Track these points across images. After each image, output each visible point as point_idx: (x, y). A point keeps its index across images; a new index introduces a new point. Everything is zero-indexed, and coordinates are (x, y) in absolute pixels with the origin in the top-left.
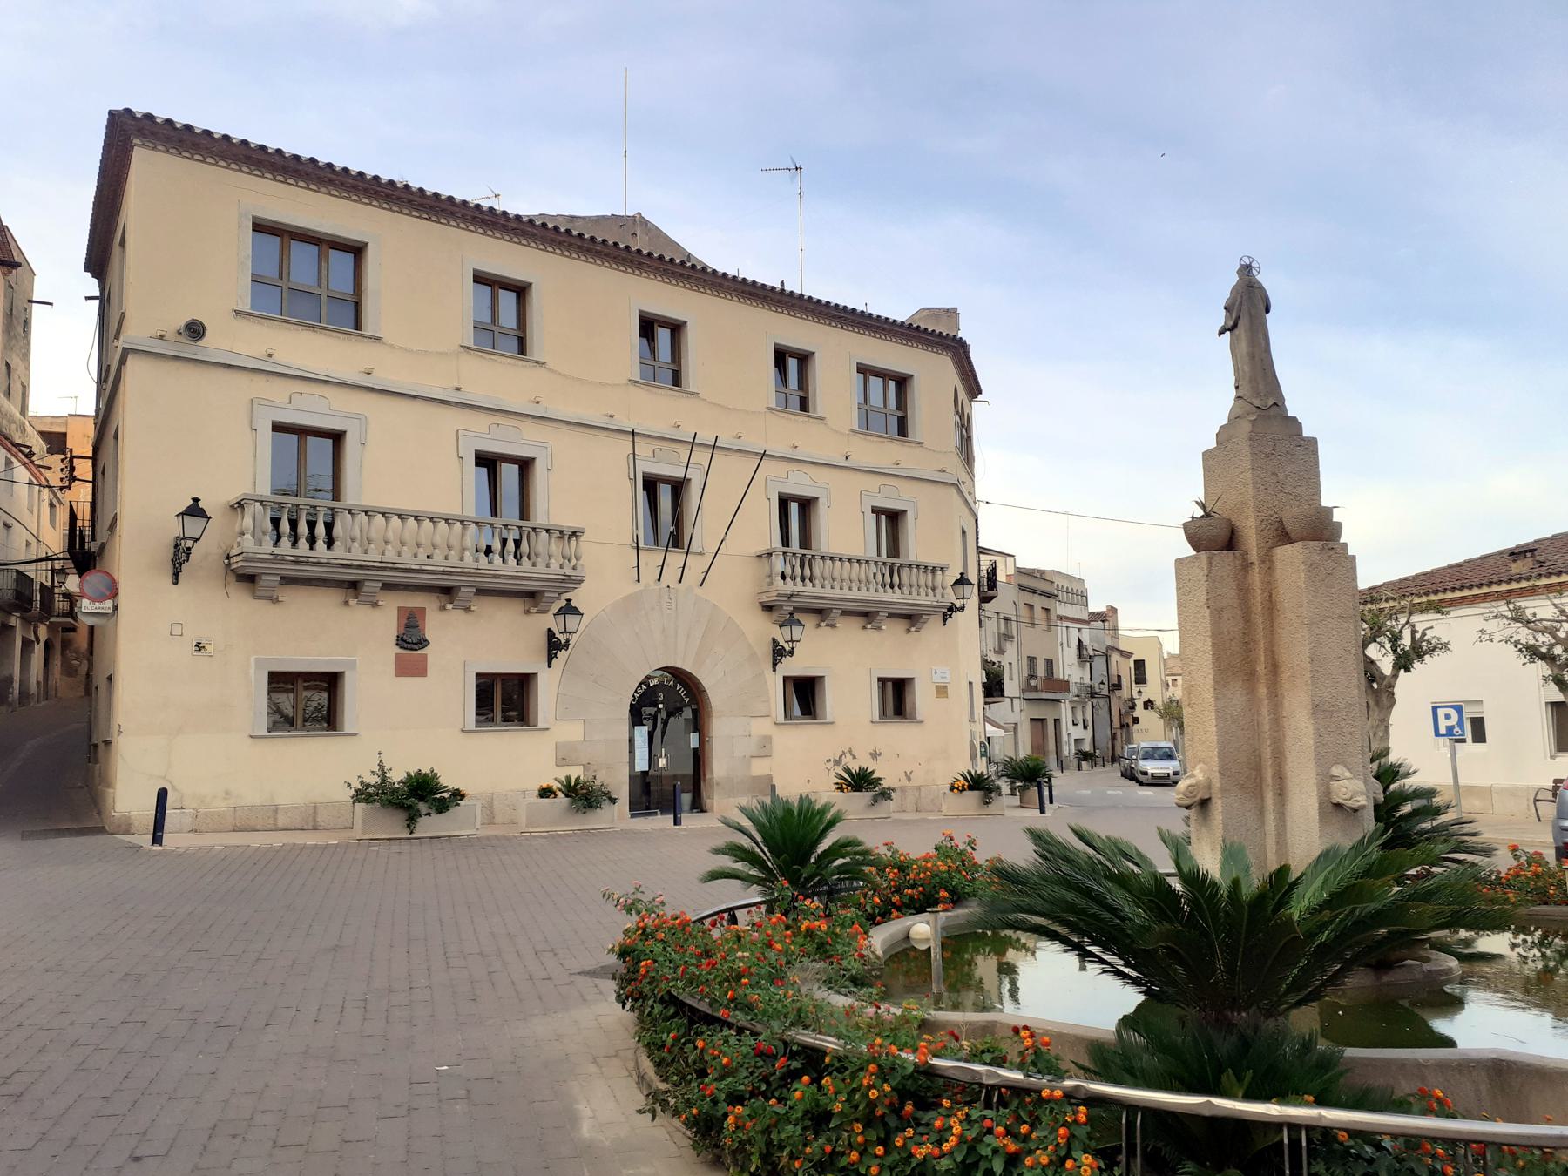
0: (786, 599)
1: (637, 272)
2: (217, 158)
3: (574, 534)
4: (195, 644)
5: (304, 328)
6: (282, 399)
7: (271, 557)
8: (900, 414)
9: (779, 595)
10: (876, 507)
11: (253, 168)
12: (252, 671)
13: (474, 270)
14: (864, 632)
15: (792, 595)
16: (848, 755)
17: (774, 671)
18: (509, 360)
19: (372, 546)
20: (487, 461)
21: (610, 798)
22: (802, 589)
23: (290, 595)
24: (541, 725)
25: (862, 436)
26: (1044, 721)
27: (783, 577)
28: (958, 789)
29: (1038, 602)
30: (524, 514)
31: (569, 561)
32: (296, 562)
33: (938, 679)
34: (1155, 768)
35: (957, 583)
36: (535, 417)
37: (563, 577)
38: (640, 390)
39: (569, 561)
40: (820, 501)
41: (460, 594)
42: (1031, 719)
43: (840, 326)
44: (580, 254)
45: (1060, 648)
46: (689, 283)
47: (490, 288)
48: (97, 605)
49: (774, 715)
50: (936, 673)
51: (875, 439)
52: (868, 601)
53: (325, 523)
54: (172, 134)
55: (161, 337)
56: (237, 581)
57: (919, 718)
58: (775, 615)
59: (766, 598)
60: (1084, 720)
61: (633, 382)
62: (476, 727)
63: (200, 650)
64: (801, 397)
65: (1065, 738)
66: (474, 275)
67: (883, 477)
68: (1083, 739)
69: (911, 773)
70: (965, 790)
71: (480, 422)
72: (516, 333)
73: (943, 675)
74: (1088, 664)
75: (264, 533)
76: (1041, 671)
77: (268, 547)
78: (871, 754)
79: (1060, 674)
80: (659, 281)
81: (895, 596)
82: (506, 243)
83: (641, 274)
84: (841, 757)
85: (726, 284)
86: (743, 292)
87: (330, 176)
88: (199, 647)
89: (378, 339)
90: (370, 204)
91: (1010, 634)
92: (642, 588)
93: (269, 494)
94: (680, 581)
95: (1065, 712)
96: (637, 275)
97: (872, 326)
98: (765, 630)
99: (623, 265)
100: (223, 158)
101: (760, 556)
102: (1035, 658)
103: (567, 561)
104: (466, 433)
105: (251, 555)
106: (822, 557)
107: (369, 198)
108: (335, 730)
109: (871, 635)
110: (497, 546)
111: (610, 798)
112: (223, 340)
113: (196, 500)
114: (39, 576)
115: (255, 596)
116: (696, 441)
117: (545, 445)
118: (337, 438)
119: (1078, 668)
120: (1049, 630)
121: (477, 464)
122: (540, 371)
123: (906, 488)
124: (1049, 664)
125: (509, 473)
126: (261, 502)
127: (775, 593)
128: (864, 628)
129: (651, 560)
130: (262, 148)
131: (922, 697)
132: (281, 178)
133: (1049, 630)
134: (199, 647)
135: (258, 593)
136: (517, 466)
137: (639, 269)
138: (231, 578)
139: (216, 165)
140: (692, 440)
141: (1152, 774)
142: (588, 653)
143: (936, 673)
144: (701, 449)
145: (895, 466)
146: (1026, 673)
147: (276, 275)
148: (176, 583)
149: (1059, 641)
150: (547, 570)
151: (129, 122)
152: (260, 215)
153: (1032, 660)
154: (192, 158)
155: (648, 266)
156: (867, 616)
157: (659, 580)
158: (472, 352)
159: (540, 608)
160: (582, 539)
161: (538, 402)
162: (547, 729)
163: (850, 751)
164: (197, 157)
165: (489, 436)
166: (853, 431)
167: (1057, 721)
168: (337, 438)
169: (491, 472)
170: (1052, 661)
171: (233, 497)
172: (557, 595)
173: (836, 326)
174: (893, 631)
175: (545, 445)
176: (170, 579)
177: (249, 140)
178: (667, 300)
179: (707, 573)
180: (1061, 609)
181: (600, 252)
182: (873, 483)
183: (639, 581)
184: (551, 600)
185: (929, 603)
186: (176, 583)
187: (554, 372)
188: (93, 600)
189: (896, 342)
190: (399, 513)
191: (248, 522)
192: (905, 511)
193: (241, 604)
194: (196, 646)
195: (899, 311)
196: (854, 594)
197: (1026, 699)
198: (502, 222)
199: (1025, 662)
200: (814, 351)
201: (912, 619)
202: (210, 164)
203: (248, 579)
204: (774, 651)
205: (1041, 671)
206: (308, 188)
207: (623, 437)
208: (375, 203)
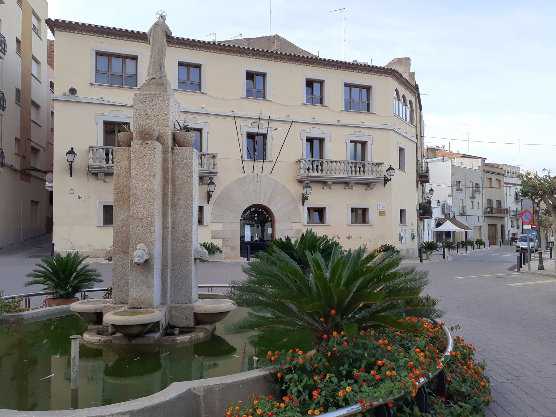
0: (306, 178)
1: (245, 56)
2: (83, 32)
3: (380, 164)
4: (78, 196)
5: (114, 88)
6: (107, 113)
7: (209, 172)
8: (367, 102)
9: (302, 177)
10: (308, 137)
11: (95, 33)
12: (98, 205)
13: (179, 62)
14: (324, 190)
15: (308, 177)
16: (336, 237)
17: (303, 205)
18: (192, 93)
19: (374, 173)
20: (310, 140)
21: (220, 251)
22: (313, 174)
23: (334, 187)
24: (205, 224)
25: (346, 112)
26: (496, 225)
27: (308, 169)
28: (377, 251)
29: (494, 177)
30: (321, 156)
31: (379, 173)
32: (108, 168)
33: (381, 208)
34: (522, 245)
35: (388, 169)
36: (202, 113)
37: (209, 172)
38: (247, 101)
39: (379, 173)
40: (326, 139)
41: (328, 184)
42: (488, 225)
43: (337, 69)
44: (221, 51)
45: (505, 196)
46: (267, 58)
47: (187, 67)
48: (50, 184)
49: (303, 222)
50: (380, 206)
51: (353, 113)
52: (344, 178)
53: (316, 165)
54: (65, 25)
55: (64, 95)
56: (92, 175)
57: (370, 223)
58: (304, 184)
59: (299, 178)
60: (517, 225)
61: (243, 98)
62: (103, 225)
63: (79, 198)
64: (368, 103)
65: (507, 232)
66: (306, 80)
67: (356, 128)
68: (517, 233)
69: (366, 245)
70: (381, 252)
71: (307, 128)
72: (320, 97)
73: (383, 207)
74: (521, 202)
75: (103, 159)
76: (495, 206)
77: (104, 163)
78: (347, 237)
79: (505, 206)
80: (255, 58)
81: (356, 175)
82: (279, 63)
83: (340, 69)
84: (333, 238)
85: (283, 57)
86: (291, 59)
87: (122, 33)
88: (79, 197)
89: (270, 101)
90: (138, 42)
91: (479, 190)
92: (246, 175)
93: (103, 145)
94: (262, 172)
95: (507, 222)
96: (245, 57)
97: (378, 71)
98: (299, 190)
99: (239, 54)
100: (84, 31)
101: (297, 162)
102: (492, 200)
103: (378, 173)
104: (100, 114)
105: (91, 166)
106: (368, 163)
107: (137, 39)
108: (323, 224)
109: (348, 191)
110: (311, 167)
111: (220, 251)
112: (81, 94)
113: (72, 148)
114: (478, 189)
115: (98, 180)
116: (270, 119)
117: (206, 123)
118: (200, 130)
119: (515, 204)
120: (500, 189)
121: (307, 141)
122: (205, 96)
123: (367, 132)
124: (499, 203)
125: (316, 143)
126: (209, 155)
127: (300, 176)
128: (345, 188)
129: (249, 165)
130: (96, 26)
131: (372, 216)
132: (106, 36)
133: (500, 189)
134: (79, 197)
135: (99, 179)
136: (319, 141)
137: (245, 55)
138: (90, 174)
139: (82, 34)
140: (268, 119)
141: (522, 247)
142: (224, 199)
143: (380, 206)
144: (273, 122)
145: (362, 124)
146: (486, 206)
147: (107, 70)
148: (71, 176)
149: (505, 193)
150: (380, 176)
151: (51, 23)
152: (98, 50)
153: (490, 201)
154: (74, 33)
155: (249, 53)
156: (346, 184)
157: (253, 172)
158: (177, 91)
159: (370, 187)
160: (383, 166)
161: (203, 108)
162: (207, 226)
163: (337, 236)
164: (76, 32)
165: (109, 115)
166: (342, 110)
167: (503, 226)
168: (200, 130)
169: (311, 144)
170: (501, 201)
171: (297, 159)
172: (375, 184)
173: (335, 69)
174: (359, 191)
175: (206, 123)
176: (69, 175)
177: (140, 31)
178: (315, 73)
179: (273, 169)
180: (506, 180)
181: (229, 50)
182: (351, 131)
183: (244, 172)
184: (373, 185)
185: (374, 178)
186: (71, 176)
187: (210, 96)
188: (49, 182)
189: (364, 73)
190: (327, 160)
191: (302, 166)
192: (367, 141)
193: (93, 183)
194: (78, 197)
195: (382, 63)
196: (337, 175)
197: (486, 217)
198: (188, 43)
199: (486, 202)
200: (324, 80)
201: (368, 184)
202: (80, 34)
203: (95, 174)
204: (303, 198)
205: (495, 206)
206: (115, 38)
207: (231, 118)
208: (140, 41)
